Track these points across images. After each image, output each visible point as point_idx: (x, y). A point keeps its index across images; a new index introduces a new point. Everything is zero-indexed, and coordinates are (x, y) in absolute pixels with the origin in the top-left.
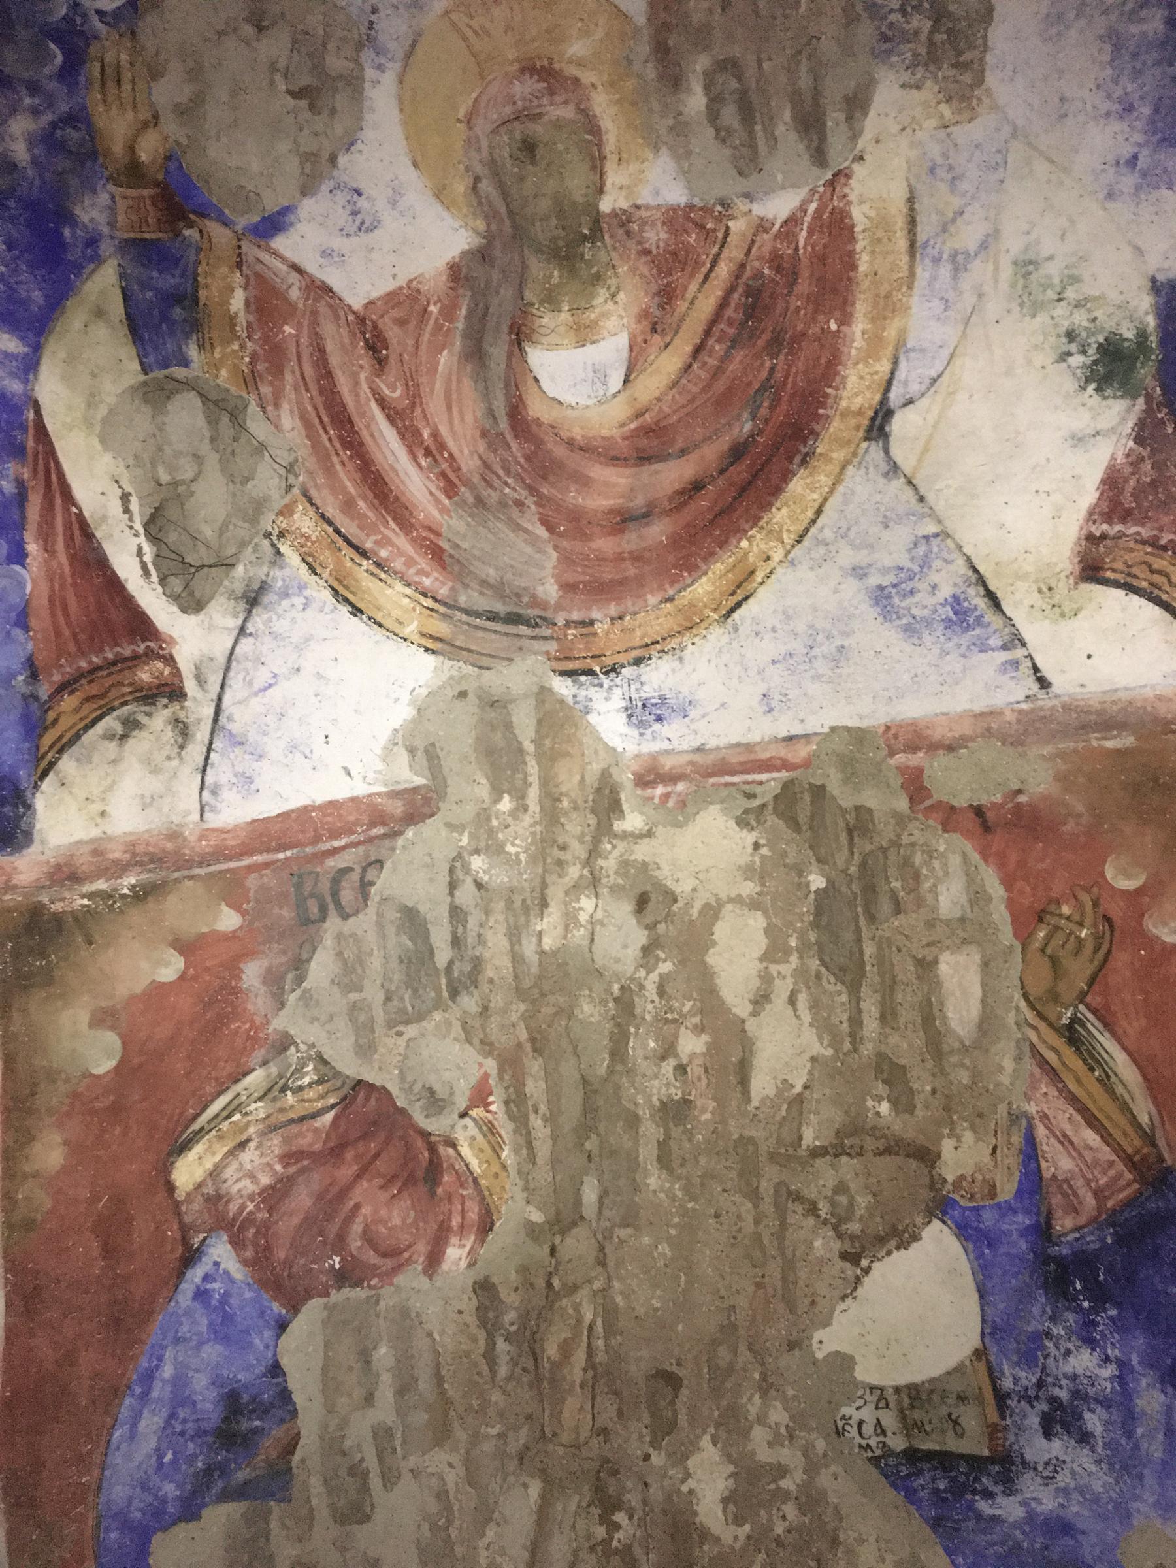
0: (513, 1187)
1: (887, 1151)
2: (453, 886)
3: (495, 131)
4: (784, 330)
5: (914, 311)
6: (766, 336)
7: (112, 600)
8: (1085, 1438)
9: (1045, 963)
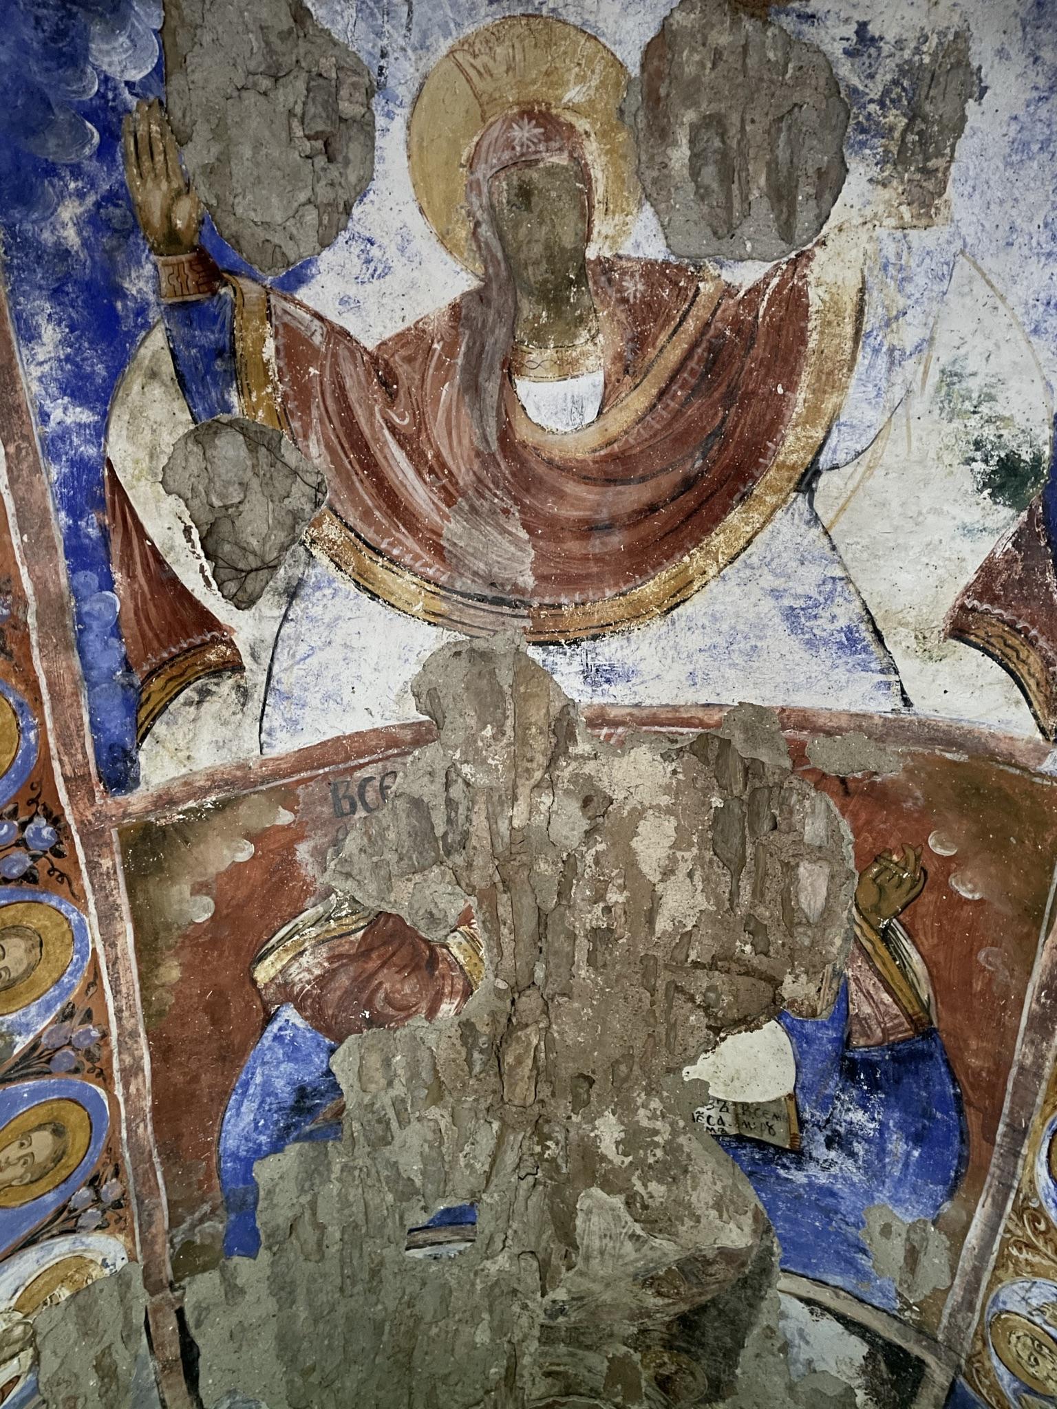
0: (487, 970)
1: (747, 974)
2: (447, 785)
3: (495, 176)
4: (737, 387)
5: (850, 391)
6: (723, 389)
7: (183, 605)
8: (852, 1155)
9: (874, 890)
